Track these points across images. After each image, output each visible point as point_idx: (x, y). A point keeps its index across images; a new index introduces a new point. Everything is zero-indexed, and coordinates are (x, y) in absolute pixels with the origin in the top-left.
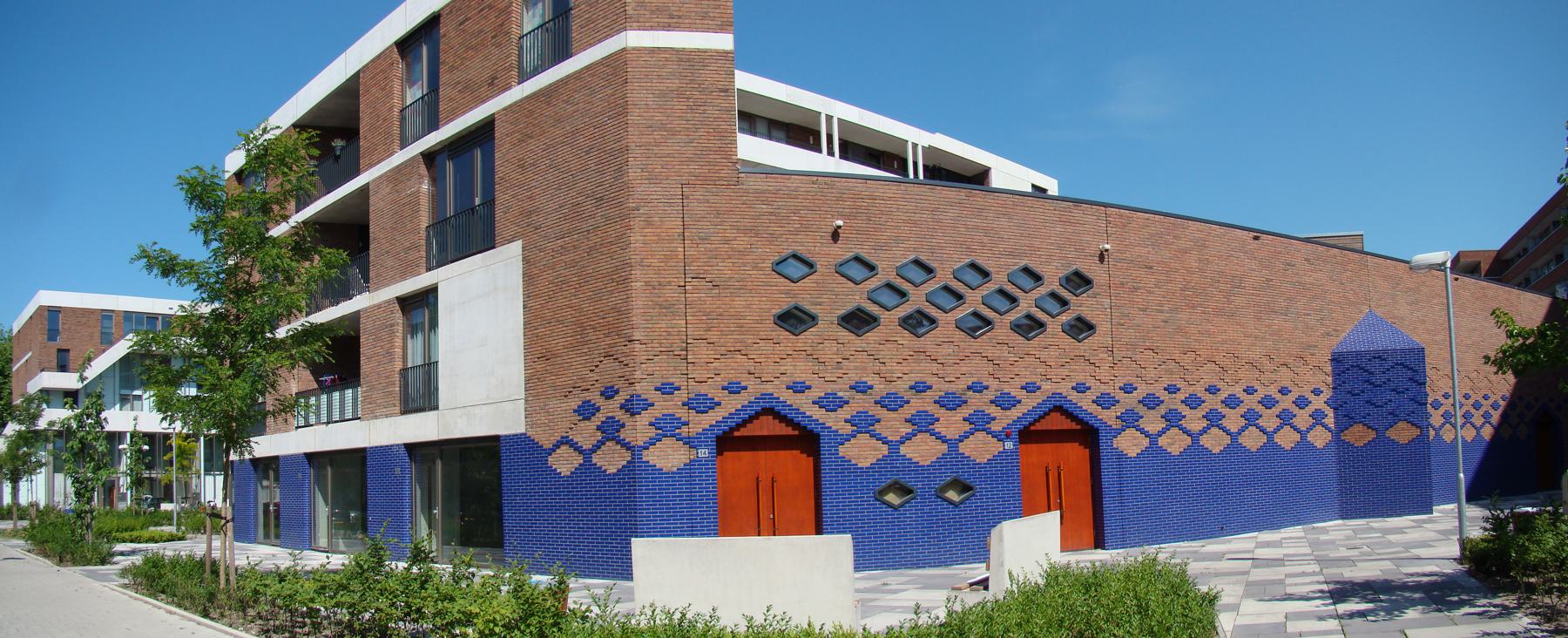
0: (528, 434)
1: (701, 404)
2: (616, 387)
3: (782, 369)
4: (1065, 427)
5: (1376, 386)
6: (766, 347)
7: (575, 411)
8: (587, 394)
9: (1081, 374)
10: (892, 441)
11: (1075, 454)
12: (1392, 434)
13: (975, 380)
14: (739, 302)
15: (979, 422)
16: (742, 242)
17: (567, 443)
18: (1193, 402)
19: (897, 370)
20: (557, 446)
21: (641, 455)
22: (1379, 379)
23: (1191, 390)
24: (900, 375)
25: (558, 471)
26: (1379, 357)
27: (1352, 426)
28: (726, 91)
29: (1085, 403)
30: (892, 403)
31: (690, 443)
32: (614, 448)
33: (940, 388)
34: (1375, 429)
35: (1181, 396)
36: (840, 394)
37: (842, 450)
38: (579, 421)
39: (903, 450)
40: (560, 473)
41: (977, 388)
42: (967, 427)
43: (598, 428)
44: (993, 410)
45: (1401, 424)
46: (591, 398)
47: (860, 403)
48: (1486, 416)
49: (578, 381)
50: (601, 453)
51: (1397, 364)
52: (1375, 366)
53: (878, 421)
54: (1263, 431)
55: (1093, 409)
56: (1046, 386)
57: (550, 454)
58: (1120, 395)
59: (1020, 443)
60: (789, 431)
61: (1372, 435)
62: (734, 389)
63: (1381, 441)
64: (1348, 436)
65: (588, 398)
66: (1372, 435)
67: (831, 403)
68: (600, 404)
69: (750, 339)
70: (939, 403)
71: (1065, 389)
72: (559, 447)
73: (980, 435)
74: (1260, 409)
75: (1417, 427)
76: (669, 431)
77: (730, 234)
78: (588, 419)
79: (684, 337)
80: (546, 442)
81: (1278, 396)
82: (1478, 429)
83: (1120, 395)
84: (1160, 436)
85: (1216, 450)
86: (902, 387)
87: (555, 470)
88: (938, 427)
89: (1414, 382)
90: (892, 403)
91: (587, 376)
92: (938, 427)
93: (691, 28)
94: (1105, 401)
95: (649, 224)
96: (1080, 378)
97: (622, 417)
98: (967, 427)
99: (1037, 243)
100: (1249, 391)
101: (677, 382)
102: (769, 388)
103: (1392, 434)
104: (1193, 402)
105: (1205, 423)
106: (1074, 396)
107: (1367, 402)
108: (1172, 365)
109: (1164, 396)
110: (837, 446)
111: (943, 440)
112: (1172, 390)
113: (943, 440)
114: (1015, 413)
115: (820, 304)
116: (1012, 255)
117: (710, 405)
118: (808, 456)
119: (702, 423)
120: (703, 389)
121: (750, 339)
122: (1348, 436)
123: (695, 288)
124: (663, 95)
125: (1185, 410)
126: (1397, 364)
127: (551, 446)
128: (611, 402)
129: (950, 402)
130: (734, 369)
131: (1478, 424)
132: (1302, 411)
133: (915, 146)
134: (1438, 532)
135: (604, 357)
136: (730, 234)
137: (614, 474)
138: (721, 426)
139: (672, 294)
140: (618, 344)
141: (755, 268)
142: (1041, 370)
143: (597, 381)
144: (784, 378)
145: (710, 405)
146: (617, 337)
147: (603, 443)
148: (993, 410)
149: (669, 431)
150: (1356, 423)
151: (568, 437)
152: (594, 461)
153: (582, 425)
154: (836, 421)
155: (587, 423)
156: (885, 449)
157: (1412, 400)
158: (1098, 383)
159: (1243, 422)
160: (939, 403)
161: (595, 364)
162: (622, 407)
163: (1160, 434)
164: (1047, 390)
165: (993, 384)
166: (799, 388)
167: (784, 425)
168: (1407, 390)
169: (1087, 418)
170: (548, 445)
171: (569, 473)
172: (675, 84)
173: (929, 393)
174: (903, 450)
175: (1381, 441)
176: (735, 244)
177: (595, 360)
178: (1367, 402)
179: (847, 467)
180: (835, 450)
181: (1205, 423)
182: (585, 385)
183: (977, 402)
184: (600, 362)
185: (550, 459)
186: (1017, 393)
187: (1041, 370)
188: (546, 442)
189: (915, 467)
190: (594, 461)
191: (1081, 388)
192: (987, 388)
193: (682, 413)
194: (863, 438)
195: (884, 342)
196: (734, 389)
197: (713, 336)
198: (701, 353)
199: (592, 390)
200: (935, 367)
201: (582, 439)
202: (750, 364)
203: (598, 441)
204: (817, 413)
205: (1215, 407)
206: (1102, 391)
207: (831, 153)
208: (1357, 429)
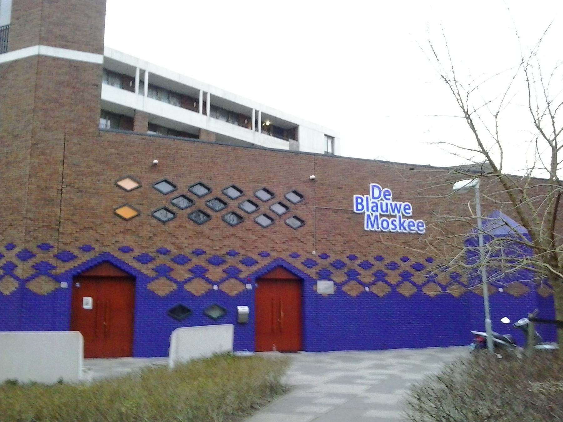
1: (66, 257)
3: (117, 239)
6: (108, 227)
9: (295, 247)
11: (290, 292)
13: (231, 249)
14: (93, 201)
15: (232, 273)
16: (97, 168)
18: (366, 265)
19: (186, 243)
23: (364, 258)
24: (187, 245)
28: (97, 86)
29: (298, 264)
30: (182, 260)
31: (57, 279)
33: (210, 253)
35: (358, 262)
36: (150, 254)
37: (150, 286)
39: (187, 287)
41: (233, 254)
42: (225, 276)
44: (241, 267)
47: (161, 260)
53: (172, 270)
54: (414, 284)
55: (301, 267)
56: (274, 254)
58: (319, 261)
62: (87, 249)
67: (145, 259)
69: (98, 221)
70: (57, 257)
71: (285, 256)
73: (232, 281)
74: (412, 271)
77: (92, 163)
79: (58, 218)
81: (425, 263)
83: (319, 261)
85: (381, 295)
86: (187, 252)
88: (172, 275)
90: (182, 260)
93: (79, 49)
94: (310, 263)
95: (43, 153)
96: (295, 250)
98: (225, 276)
99: (272, 176)
100: (405, 259)
101: (51, 243)
102: (107, 250)
104: (366, 265)
105: (373, 279)
106: (290, 260)
108: (353, 243)
109: (347, 262)
111: (176, 282)
112: (352, 258)
113: (176, 282)
114: (254, 268)
115: (142, 204)
116: (257, 181)
117: (253, 262)
119: (63, 268)
120: (68, 248)
121: (98, 221)
123: (68, 192)
124: (60, 83)
125: (361, 271)
129: (216, 261)
130: (87, 237)
132: (418, 273)
133: (257, 112)
136: (92, 163)
139: (53, 194)
141: (105, 182)
142: (271, 245)
144: (118, 245)
145: (253, 262)
148: (241, 267)
154: (147, 270)
156: (175, 287)
158: (305, 253)
159: (400, 279)
160: (57, 257)
164: (274, 256)
165: (242, 252)
166: (126, 250)
169: (128, 269)
172: (67, 78)
173: (203, 256)
174: (187, 287)
176: (95, 169)
179: (153, 296)
181: (373, 279)
183: (231, 261)
186: (255, 257)
187: (271, 245)
189: (191, 297)
191: (295, 256)
192: (238, 254)
193: (53, 262)
194: (163, 280)
196: (87, 249)
197: (76, 218)
198: (69, 228)
200: (208, 242)
204: (136, 265)
206: (308, 257)
207: (205, 113)
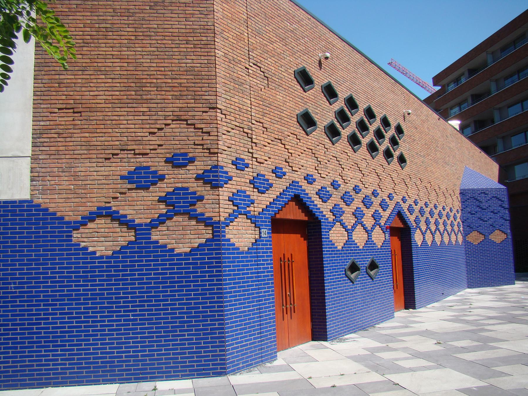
0: (36, 201)
2: (191, 155)
4: (301, 219)
5: (483, 209)
7: (122, 178)
8: (142, 160)
10: (141, 225)
12: (492, 237)
17: (108, 215)
20: (91, 217)
21: (71, 236)
22: (484, 205)
25: (91, 249)
26: (484, 193)
27: (471, 232)
32: (185, 223)
34: (484, 235)
38: (129, 189)
40: (94, 253)
42: (163, 209)
43: (161, 200)
45: (497, 232)
46: (150, 164)
48: (376, 216)
49: (130, 143)
50: (165, 228)
51: (493, 197)
52: (482, 198)
57: (77, 229)
59: (273, 232)
60: (301, 216)
61: (482, 238)
63: (486, 240)
64: (470, 238)
65: (145, 164)
66: (482, 238)
68: (166, 172)
72: (92, 220)
75: (505, 233)
76: (182, 207)
78: (146, 188)
80: (71, 213)
82: (349, 232)
84: (156, 227)
87: (86, 248)
88: (199, 208)
89: (502, 208)
91: (145, 139)
92: (199, 208)
97: (199, 189)
98: (163, 209)
103: (492, 237)
106: (304, 184)
107: (479, 218)
110: (71, 232)
118: (304, 240)
122: (470, 238)
126: (493, 197)
127: (79, 218)
128: (182, 172)
131: (369, 226)
134: (357, 359)
135: (173, 120)
137: (186, 254)
138: (187, 198)
140: (196, 109)
143: (159, 145)
146: (193, 101)
147: (170, 218)
149: (182, 207)
150: (474, 230)
151: (110, 208)
152: (154, 238)
153: (134, 195)
155: (142, 193)
157: (501, 218)
161: (158, 126)
162: (198, 178)
163: (155, 224)
167: (300, 210)
168: (499, 212)
170: (71, 216)
171: (246, 249)
175: (486, 240)
177: (159, 122)
178: (479, 218)
180: (67, 236)
182: (139, 148)
184: (166, 125)
185: (75, 235)
188: (71, 213)
190: (154, 238)
195: (207, 109)
199: (150, 155)
201: (132, 212)
202: (190, 130)
203: (161, 215)
205: (243, 188)
208: (475, 234)
